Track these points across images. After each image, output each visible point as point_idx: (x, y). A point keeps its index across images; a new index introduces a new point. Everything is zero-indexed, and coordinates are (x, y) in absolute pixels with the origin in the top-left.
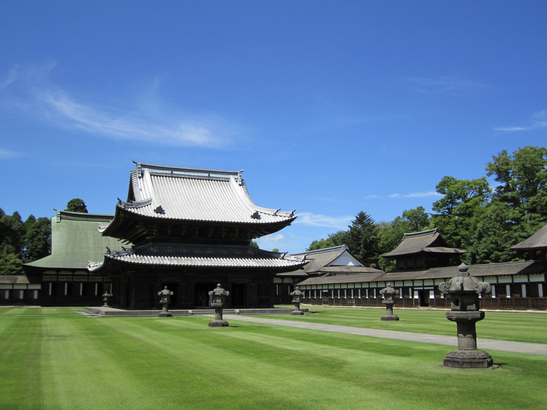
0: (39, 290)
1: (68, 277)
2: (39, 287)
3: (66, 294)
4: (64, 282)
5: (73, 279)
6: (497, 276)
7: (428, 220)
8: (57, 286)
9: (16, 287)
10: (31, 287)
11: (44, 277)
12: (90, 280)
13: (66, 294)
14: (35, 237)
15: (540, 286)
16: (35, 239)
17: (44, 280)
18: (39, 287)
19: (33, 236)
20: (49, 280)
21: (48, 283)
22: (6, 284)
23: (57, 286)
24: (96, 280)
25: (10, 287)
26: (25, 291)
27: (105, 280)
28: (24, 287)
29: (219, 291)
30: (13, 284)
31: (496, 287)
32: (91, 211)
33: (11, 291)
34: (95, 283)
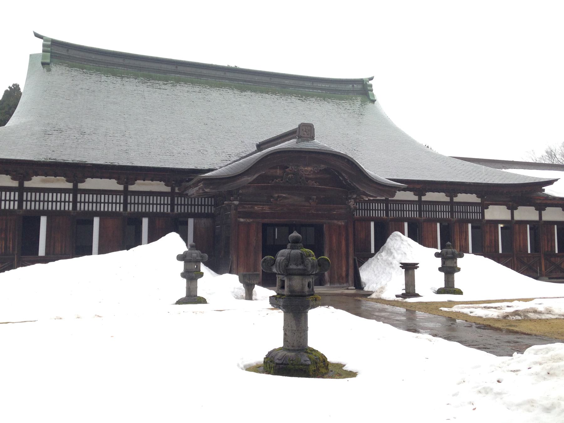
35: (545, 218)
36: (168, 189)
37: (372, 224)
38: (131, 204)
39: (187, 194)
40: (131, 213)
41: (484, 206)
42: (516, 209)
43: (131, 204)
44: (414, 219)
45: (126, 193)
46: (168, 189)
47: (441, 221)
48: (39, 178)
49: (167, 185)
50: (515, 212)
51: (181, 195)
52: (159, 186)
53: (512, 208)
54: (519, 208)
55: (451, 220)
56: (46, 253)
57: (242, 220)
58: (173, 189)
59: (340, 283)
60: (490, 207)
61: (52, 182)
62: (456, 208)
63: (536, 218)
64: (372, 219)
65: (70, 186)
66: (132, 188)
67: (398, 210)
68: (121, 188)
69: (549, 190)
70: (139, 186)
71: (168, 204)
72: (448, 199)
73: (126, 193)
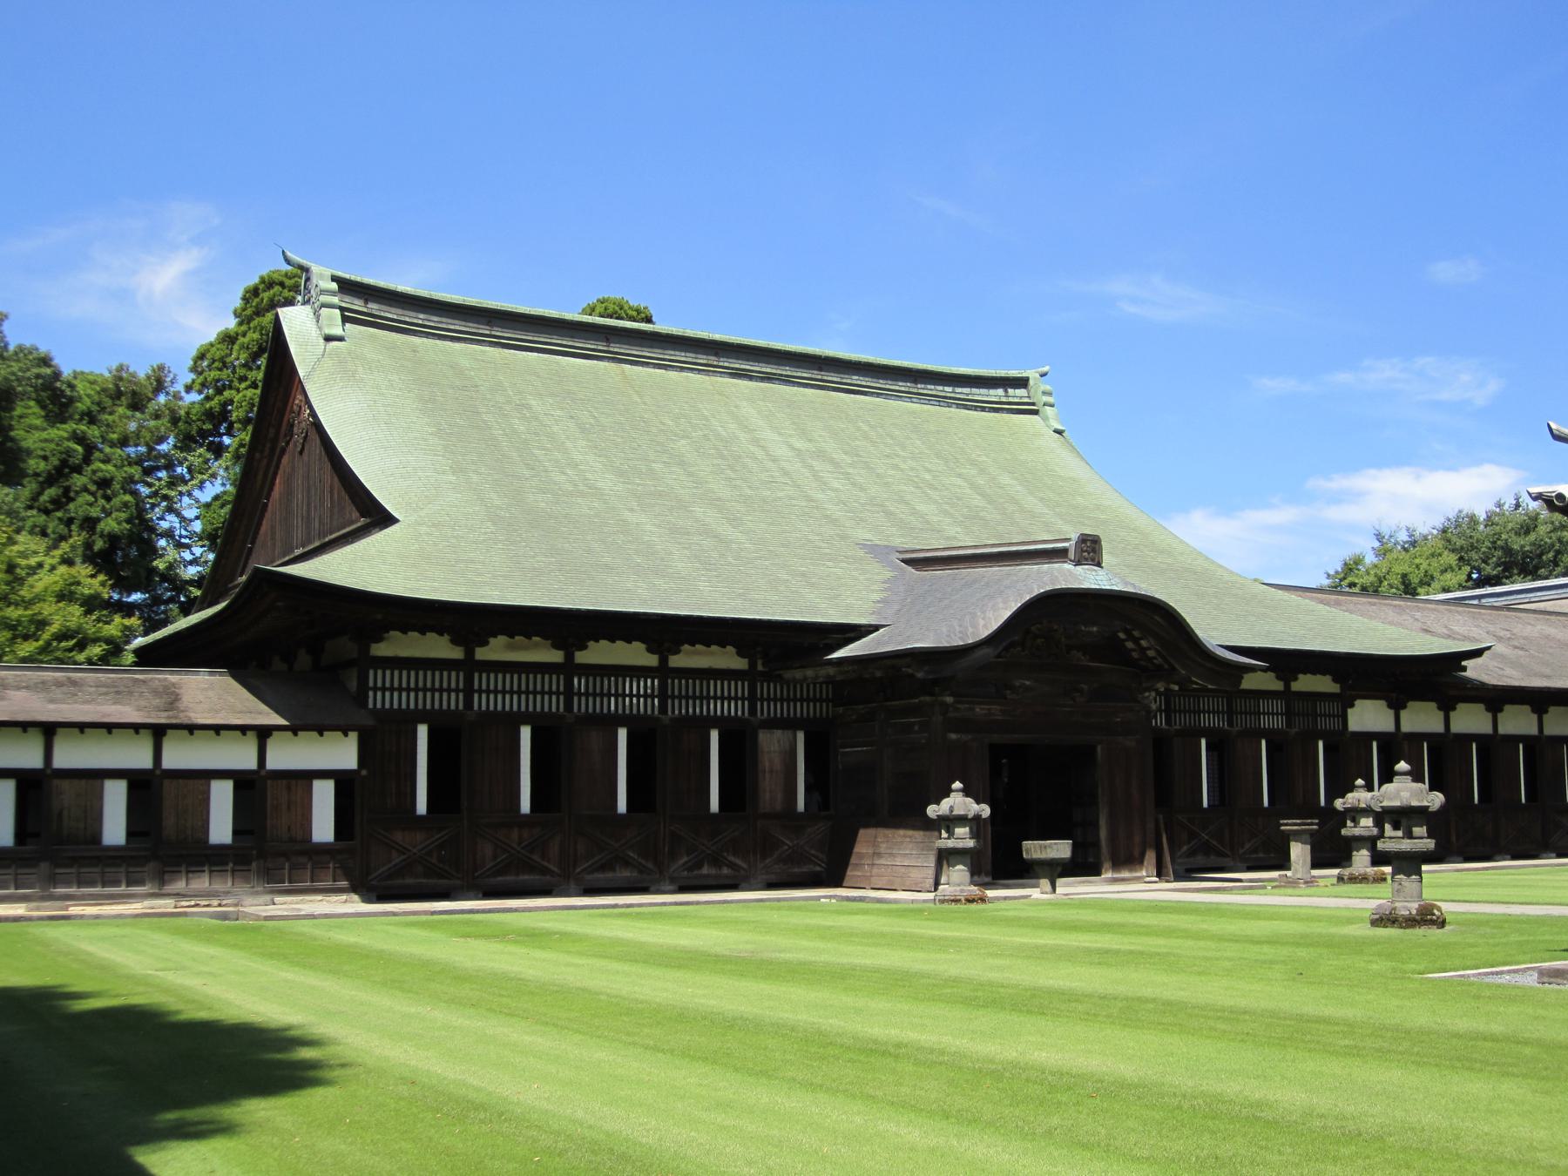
0: (341, 779)
1: (539, 681)
2: (342, 753)
3: (525, 805)
4: (512, 722)
5: (469, 692)
6: (49, 730)
7: (12, 418)
8: (465, 748)
9: (178, 755)
10: (287, 755)
11: (375, 677)
12: (481, 703)
13: (525, 805)
14: (78, 470)
15: (324, 796)
16: (78, 481)
17: (376, 700)
18: (342, 753)
19: (64, 463)
20: (408, 701)
21: (405, 722)
22: (110, 727)
23: (465, 748)
24: (718, 708)
25: (138, 756)
26: (247, 785)
27: (765, 711)
28: (243, 756)
29: (957, 802)
30: (158, 732)
31: (237, 789)
32: (338, 311)
33: (142, 786)
34: (702, 725)
35: (1548, 731)
36: (740, 664)
37: (714, 736)
38: (480, 691)
39: (780, 676)
40: (481, 714)
41: (1345, 701)
42: (1405, 707)
43: (480, 691)
44: (644, 718)
45: (569, 669)
46: (740, 664)
47: (1270, 735)
48: (502, 640)
49: (650, 650)
50: (1404, 714)
51: (768, 677)
52: (726, 658)
53: (1397, 706)
54: (1410, 704)
55: (658, 719)
56: (131, 833)
57: (953, 736)
58: (752, 664)
59: (1118, 864)
60: (1358, 703)
61: (526, 648)
62: (676, 685)
63: (1533, 730)
64: (616, 721)
65: (556, 656)
66: (676, 661)
67: (512, 692)
68: (457, 653)
69: (1474, 670)
70: (496, 650)
71: (743, 699)
72: (1278, 686)
73: (663, 672)
